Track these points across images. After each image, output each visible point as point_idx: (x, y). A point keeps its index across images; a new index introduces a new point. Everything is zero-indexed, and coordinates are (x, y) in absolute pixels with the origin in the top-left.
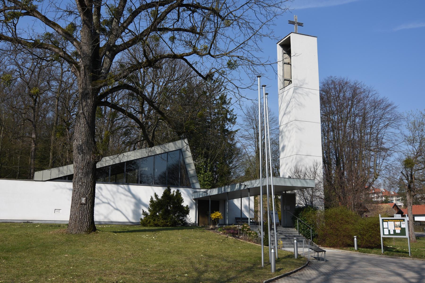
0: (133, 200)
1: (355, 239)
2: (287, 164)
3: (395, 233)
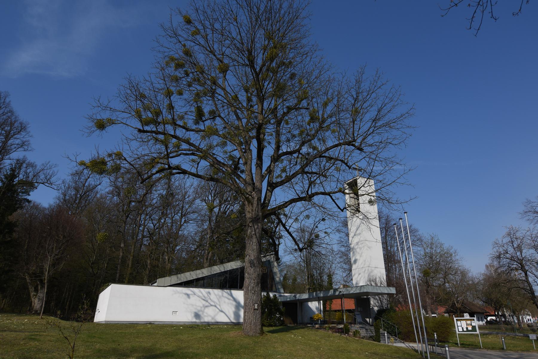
0: (234, 303)
2: (360, 274)
3: (468, 330)
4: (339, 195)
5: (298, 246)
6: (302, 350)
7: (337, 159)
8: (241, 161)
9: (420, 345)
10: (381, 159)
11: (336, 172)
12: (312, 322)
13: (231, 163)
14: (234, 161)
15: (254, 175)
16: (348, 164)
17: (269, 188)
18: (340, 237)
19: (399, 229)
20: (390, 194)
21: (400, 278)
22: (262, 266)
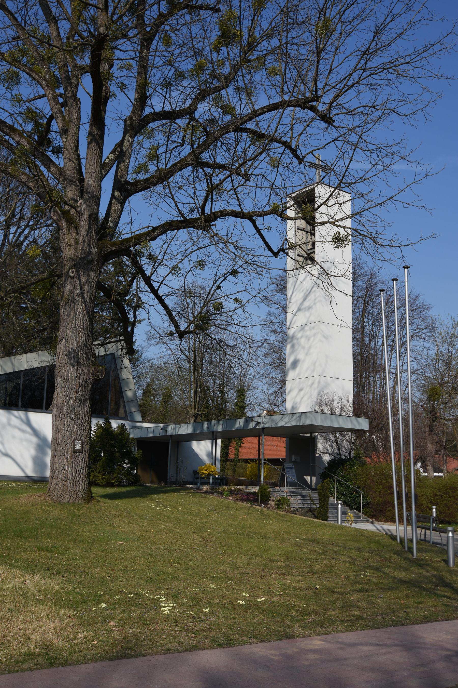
0: (34, 440)
1: (434, 510)
2: (301, 390)
4: (272, 220)
5: (177, 326)
6: (170, 531)
7: (273, 139)
8: (55, 126)
9: (401, 528)
10: (371, 147)
11: (269, 167)
12: (197, 479)
13: (30, 127)
14: (37, 124)
15: (83, 162)
16: (298, 152)
17: (117, 194)
18: (270, 314)
19: (389, 303)
20: (379, 224)
21: (380, 401)
22: (94, 364)
